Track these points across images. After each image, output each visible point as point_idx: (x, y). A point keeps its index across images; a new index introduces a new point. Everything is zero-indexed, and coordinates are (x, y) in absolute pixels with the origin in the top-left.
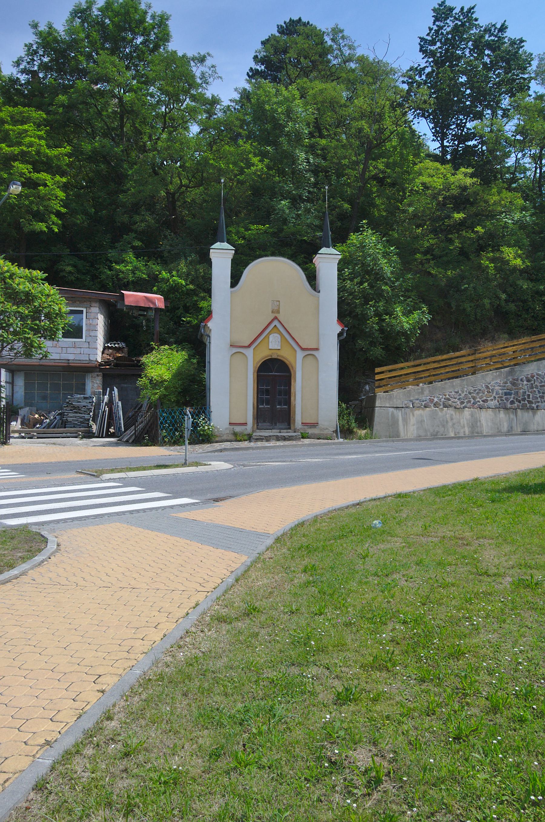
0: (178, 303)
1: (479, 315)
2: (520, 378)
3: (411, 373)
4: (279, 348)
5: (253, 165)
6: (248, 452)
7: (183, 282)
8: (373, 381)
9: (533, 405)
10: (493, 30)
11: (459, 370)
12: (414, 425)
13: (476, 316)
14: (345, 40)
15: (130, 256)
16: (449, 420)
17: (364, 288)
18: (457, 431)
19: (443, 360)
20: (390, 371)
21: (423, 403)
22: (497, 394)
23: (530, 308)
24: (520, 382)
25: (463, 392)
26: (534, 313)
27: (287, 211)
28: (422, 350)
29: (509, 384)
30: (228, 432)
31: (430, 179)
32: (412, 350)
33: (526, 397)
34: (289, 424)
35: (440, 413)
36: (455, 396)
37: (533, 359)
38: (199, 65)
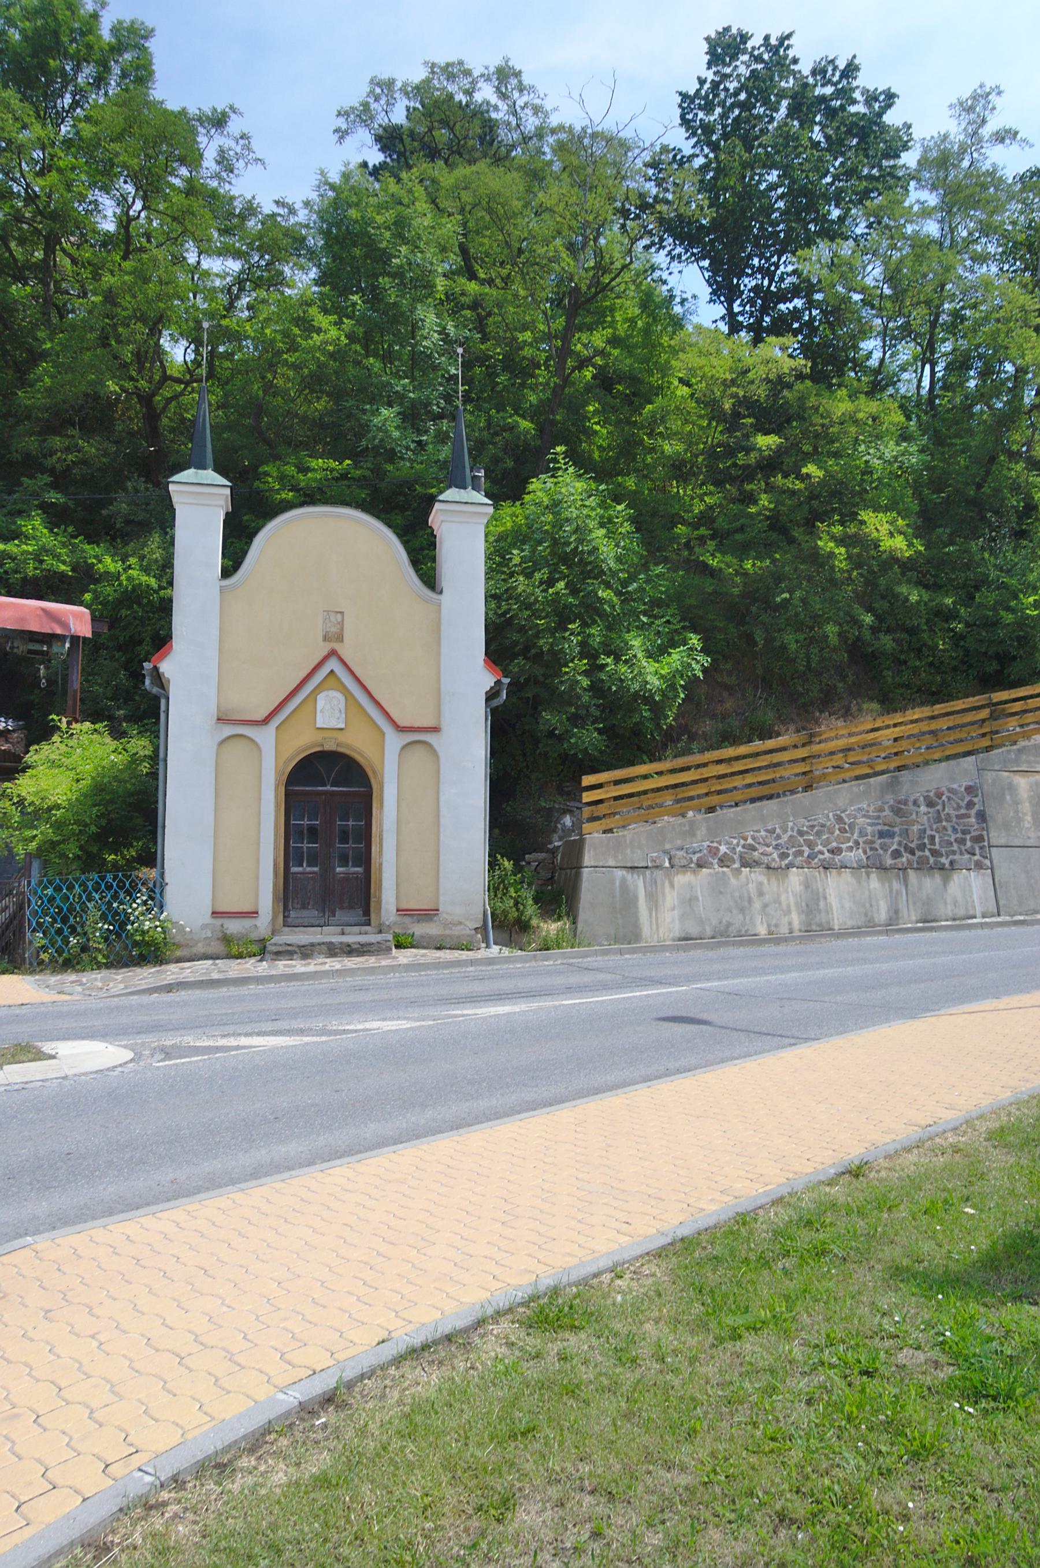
0: (140, 629)
1: (815, 659)
2: (912, 798)
3: (667, 787)
4: (342, 726)
5: (319, 331)
6: (243, 990)
7: (153, 582)
8: (580, 806)
9: (943, 860)
10: (830, 72)
11: (774, 781)
12: (673, 909)
13: (808, 662)
14: (525, 92)
15: (35, 525)
16: (754, 896)
17: (557, 593)
18: (774, 922)
19: (737, 758)
20: (617, 783)
21: (695, 858)
22: (862, 834)
23: (925, 645)
24: (911, 806)
25: (785, 831)
26: (934, 657)
27: (396, 434)
28: (692, 737)
29: (887, 812)
30: (209, 934)
31: (702, 361)
32: (670, 737)
33: (926, 841)
34: (367, 913)
35: (733, 881)
36: (768, 841)
37: (936, 757)
38: (213, 131)
